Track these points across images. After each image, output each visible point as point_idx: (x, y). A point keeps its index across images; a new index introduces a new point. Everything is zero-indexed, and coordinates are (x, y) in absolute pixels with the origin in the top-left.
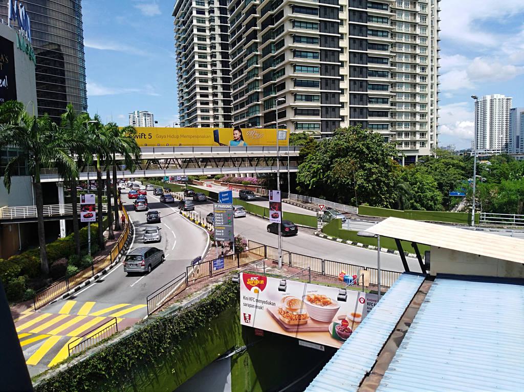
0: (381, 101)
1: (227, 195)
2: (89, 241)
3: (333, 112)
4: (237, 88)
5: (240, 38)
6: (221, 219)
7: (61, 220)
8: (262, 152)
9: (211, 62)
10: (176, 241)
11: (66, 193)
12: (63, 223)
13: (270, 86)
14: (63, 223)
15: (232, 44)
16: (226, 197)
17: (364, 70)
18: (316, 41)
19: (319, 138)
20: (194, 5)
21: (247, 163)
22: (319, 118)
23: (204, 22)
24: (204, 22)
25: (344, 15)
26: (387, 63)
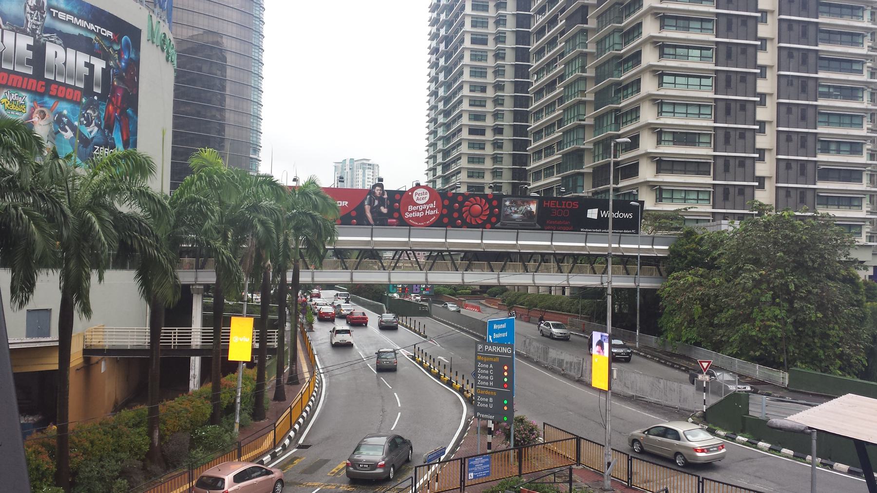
0: (847, 148)
1: (504, 326)
2: (238, 400)
3: (741, 169)
4: (543, 97)
5: (553, 21)
6: (489, 375)
7: (192, 358)
8: (650, 247)
9: (495, 51)
10: (399, 414)
11: (205, 307)
12: (196, 362)
13: (609, 87)
14: (196, 362)
15: (536, 33)
16: (502, 331)
17: (810, 167)
18: (709, 25)
19: (709, 220)
20: (468, 10)
21: (553, 264)
22: (708, 180)
23: (483, 89)
24: (484, 42)
25: (767, 30)
26: (860, 72)
